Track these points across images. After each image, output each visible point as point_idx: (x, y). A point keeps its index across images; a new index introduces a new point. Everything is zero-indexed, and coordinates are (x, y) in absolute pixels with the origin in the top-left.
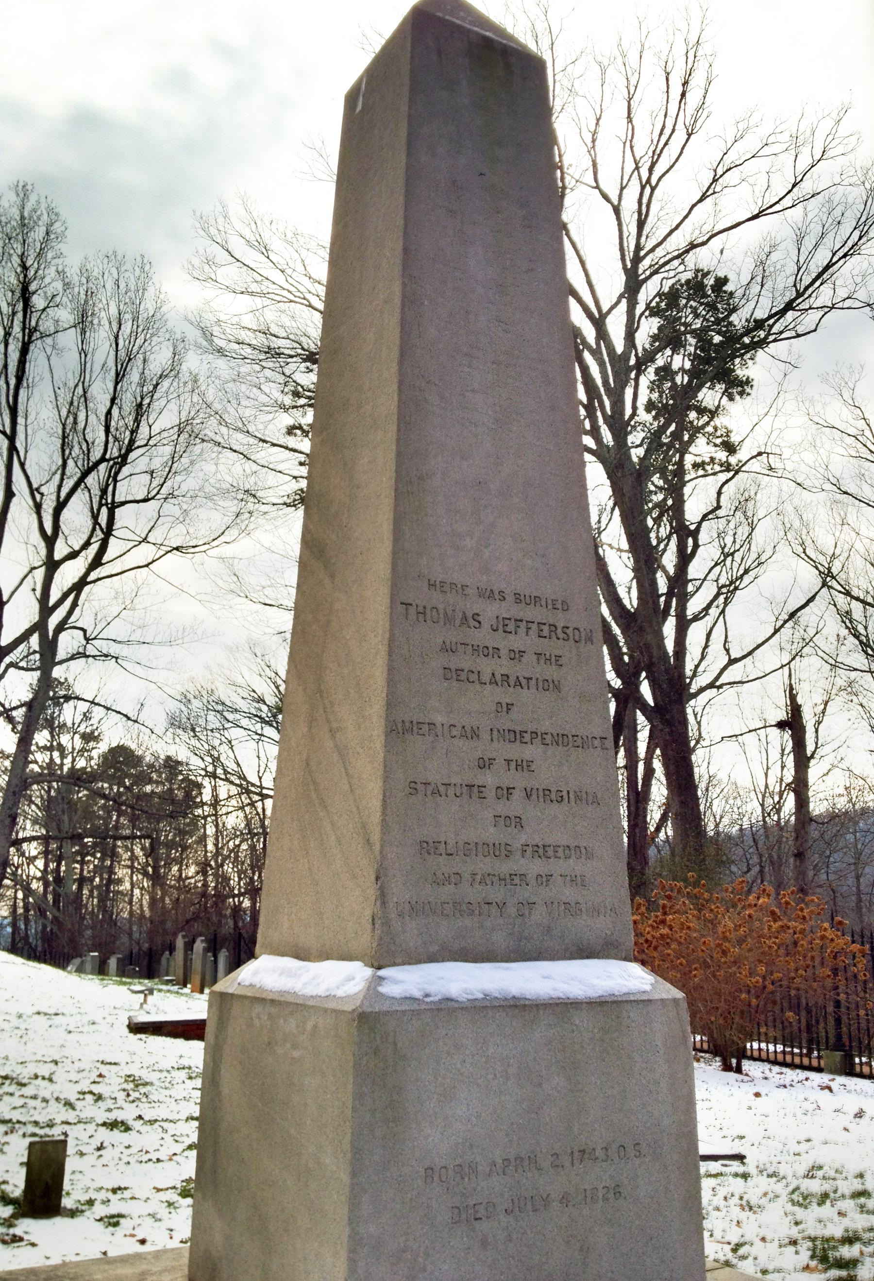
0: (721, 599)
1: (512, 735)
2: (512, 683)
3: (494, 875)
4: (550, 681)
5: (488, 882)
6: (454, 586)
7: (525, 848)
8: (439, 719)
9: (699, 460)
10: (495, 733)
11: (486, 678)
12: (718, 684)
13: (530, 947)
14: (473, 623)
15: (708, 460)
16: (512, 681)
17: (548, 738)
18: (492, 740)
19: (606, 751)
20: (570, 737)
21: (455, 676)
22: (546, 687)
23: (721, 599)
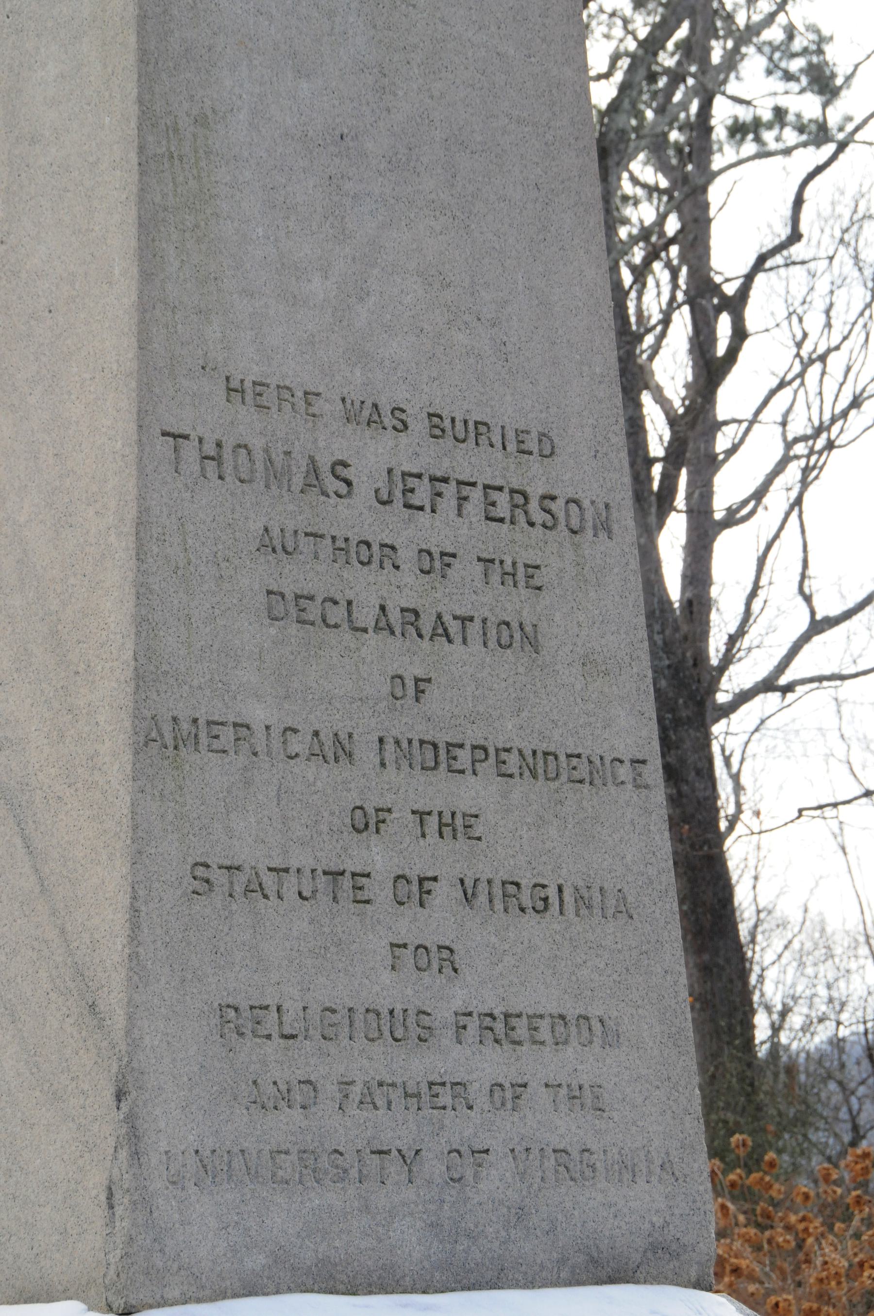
0: (793, 471)
1: (429, 754)
2: (427, 631)
3: (393, 1085)
4: (515, 625)
5: (379, 1103)
6: (286, 395)
7: (463, 1020)
9: (744, 114)
10: (390, 747)
12: (783, 681)
13: (478, 1256)
14: (333, 485)
15: (767, 115)
16: (427, 624)
17: (513, 760)
18: (383, 765)
19: (644, 792)
20: (562, 758)
21: (293, 611)
22: (505, 640)
23: (793, 471)
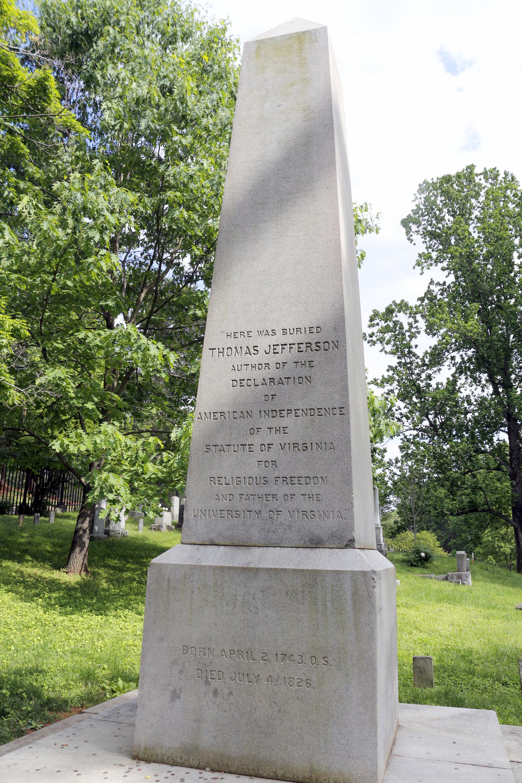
4: (304, 377)
10: (263, 413)
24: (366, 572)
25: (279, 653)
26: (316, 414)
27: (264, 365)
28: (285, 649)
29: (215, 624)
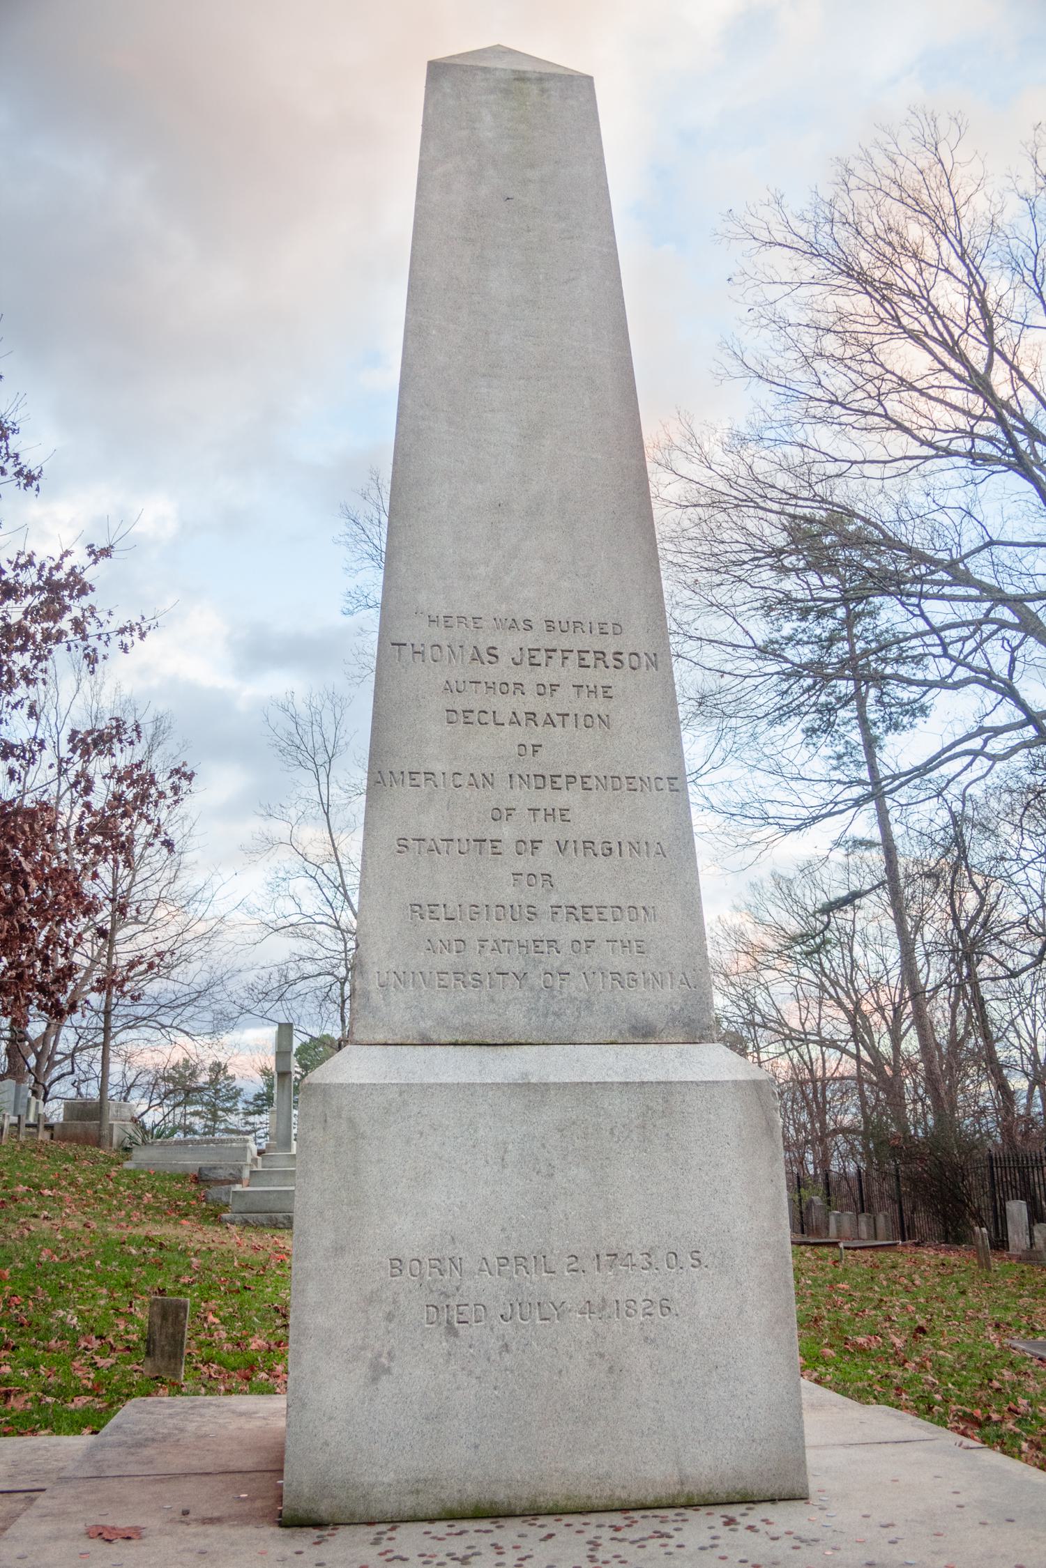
4: (595, 716)
8: (438, 768)
11: (504, 717)
14: (486, 657)
16: (540, 719)
24: (761, 1081)
25: (603, 1252)
26: (625, 788)
27: (512, 687)
28: (614, 1244)
29: (462, 1206)
